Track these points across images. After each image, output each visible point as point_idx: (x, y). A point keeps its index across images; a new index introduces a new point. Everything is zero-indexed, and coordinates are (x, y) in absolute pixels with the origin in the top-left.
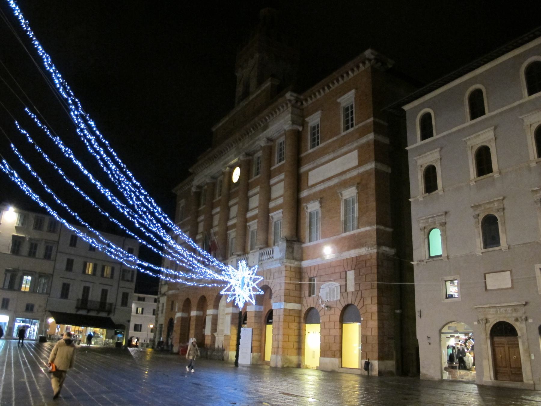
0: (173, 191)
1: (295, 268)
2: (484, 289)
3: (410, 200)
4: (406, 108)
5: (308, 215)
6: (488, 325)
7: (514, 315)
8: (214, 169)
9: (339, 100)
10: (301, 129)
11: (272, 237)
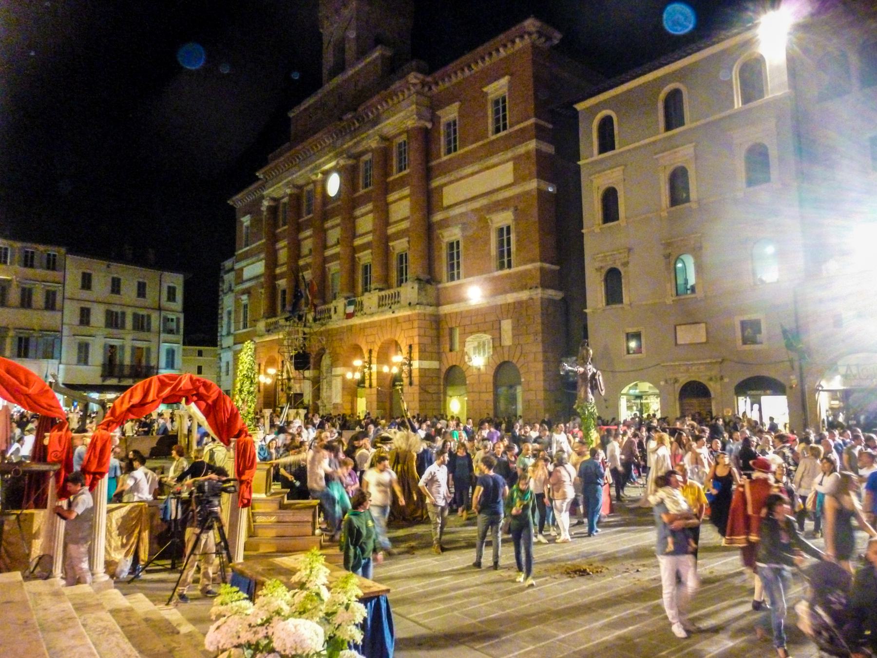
0: (230, 202)
1: (430, 315)
2: (673, 342)
3: (583, 231)
4: (580, 107)
5: (444, 246)
6: (677, 385)
7: (708, 373)
8: (299, 176)
9: (485, 90)
10: (429, 125)
11: (394, 274)
